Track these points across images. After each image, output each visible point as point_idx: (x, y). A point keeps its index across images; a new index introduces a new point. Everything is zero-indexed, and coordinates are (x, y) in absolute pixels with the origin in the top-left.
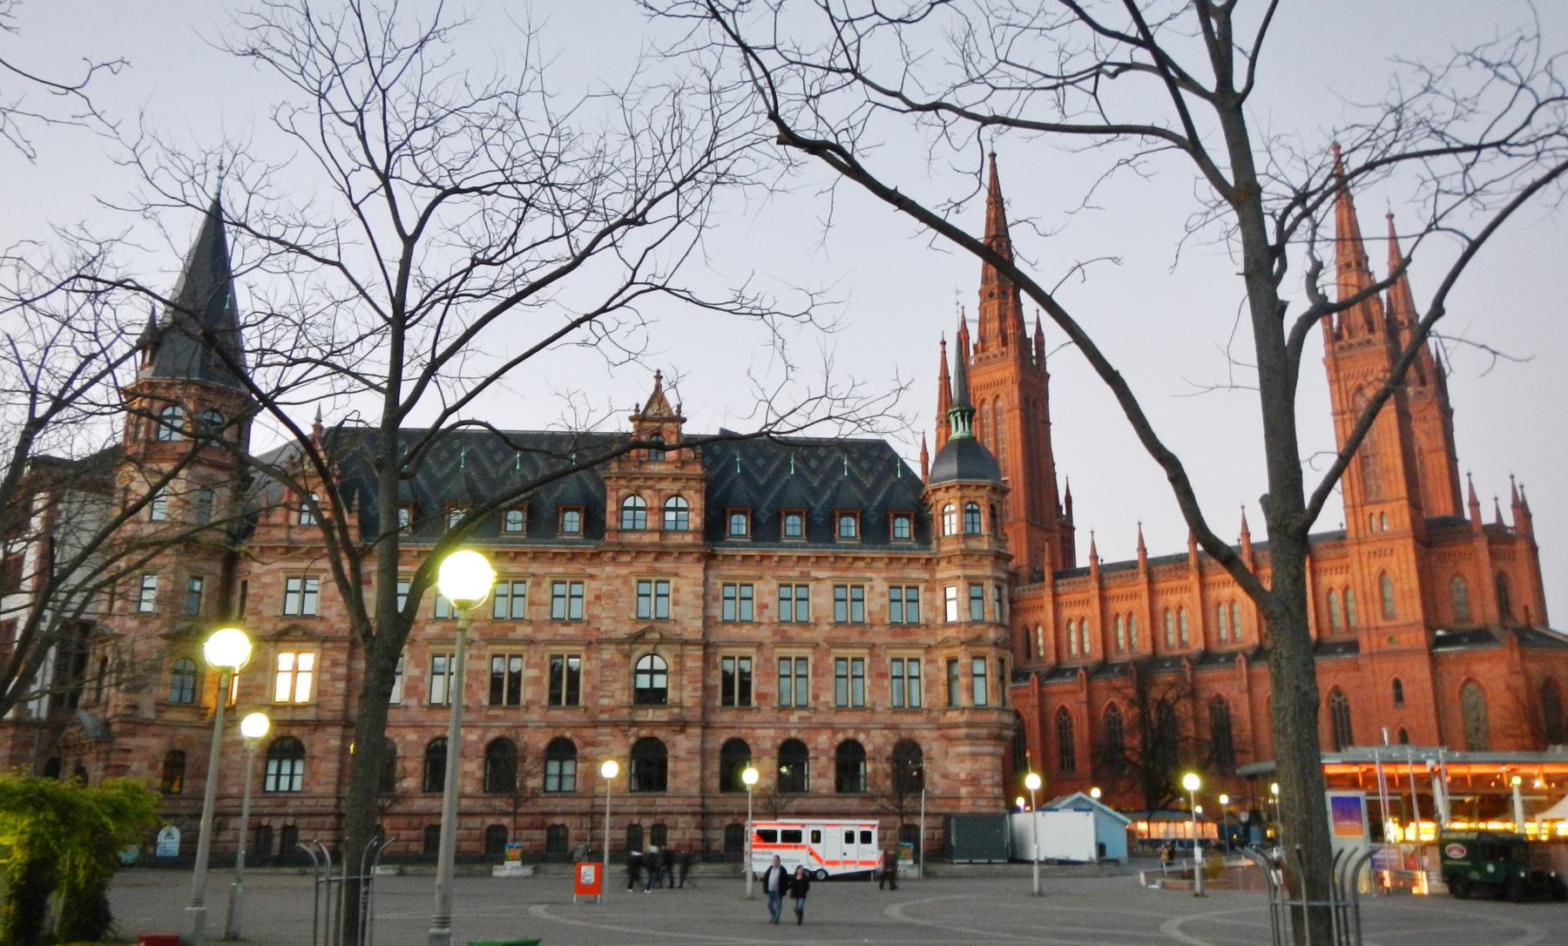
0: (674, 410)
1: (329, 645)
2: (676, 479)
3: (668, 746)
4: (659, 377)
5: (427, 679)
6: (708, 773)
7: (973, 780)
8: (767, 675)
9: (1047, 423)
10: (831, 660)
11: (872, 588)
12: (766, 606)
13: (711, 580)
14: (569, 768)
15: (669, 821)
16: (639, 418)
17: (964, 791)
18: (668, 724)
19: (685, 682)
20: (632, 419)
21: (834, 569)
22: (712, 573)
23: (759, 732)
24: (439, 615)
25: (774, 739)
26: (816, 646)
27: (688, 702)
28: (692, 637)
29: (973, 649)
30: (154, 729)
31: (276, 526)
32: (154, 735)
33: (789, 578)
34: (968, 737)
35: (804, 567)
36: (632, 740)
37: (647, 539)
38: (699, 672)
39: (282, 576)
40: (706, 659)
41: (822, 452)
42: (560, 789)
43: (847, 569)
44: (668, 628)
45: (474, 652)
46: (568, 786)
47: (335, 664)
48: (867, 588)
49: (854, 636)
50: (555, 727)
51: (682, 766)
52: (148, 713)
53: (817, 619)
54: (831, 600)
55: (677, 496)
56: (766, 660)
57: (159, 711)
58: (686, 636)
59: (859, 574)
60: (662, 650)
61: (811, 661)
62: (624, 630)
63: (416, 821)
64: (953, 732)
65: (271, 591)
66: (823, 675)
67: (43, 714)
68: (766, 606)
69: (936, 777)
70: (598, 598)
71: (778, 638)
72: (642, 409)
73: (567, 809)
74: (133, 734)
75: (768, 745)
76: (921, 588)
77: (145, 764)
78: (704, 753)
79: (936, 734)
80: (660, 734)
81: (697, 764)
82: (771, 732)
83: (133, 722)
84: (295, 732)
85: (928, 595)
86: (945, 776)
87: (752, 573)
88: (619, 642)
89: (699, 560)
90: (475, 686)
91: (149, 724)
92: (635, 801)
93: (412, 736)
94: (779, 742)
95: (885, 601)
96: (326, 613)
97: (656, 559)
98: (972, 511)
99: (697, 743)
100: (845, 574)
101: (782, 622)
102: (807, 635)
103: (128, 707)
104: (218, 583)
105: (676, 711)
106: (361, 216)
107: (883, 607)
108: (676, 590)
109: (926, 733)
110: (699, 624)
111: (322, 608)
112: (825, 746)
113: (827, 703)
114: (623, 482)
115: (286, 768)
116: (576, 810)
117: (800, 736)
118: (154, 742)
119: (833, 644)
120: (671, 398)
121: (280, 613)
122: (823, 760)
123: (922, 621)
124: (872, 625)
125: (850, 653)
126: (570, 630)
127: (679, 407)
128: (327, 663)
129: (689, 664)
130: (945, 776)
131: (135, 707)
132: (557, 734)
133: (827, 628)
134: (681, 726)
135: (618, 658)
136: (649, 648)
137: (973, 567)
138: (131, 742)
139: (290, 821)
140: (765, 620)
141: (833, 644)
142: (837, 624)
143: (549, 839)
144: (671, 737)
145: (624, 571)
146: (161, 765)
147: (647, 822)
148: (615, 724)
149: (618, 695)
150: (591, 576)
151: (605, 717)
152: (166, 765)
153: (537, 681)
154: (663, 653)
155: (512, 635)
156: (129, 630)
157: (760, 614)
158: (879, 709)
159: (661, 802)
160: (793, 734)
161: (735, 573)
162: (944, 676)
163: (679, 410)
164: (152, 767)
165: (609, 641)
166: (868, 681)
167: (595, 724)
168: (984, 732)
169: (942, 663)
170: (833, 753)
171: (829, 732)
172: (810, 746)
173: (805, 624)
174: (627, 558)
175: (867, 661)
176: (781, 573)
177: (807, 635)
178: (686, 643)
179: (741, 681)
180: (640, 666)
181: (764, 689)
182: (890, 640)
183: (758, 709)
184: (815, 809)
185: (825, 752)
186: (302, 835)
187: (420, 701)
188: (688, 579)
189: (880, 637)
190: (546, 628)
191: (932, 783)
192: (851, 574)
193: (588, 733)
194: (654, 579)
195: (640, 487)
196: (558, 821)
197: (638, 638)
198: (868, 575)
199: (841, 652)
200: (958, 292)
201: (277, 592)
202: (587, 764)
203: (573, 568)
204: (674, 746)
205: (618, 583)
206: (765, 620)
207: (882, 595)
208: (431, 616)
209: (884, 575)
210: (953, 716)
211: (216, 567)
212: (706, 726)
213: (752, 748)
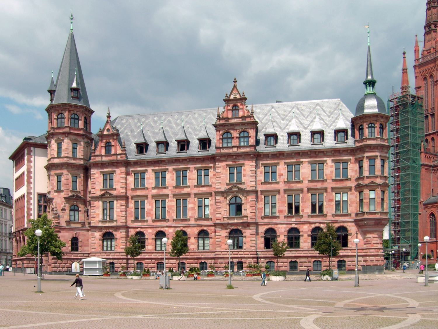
8: (282, 202)
9: (82, 74)
12: (282, 175)
24: (374, 192)
27: (250, 215)
46: (206, 248)
52: (63, 224)
54: (310, 170)
57: (67, 224)
66: (306, 202)
68: (282, 175)
72: (228, 96)
74: (60, 232)
84: (205, 228)
90: (171, 211)
91: (63, 229)
98: (74, 119)
115: (109, 243)
122: (305, 236)
128: (119, 205)
131: (59, 223)
139: (111, 261)
151: (218, 222)
153: (193, 209)
156: (55, 196)
159: (241, 254)
179: (295, 206)
181: (281, 208)
183: (279, 217)
186: (116, 265)
187: (152, 218)
200: (72, 19)
207: (332, 167)
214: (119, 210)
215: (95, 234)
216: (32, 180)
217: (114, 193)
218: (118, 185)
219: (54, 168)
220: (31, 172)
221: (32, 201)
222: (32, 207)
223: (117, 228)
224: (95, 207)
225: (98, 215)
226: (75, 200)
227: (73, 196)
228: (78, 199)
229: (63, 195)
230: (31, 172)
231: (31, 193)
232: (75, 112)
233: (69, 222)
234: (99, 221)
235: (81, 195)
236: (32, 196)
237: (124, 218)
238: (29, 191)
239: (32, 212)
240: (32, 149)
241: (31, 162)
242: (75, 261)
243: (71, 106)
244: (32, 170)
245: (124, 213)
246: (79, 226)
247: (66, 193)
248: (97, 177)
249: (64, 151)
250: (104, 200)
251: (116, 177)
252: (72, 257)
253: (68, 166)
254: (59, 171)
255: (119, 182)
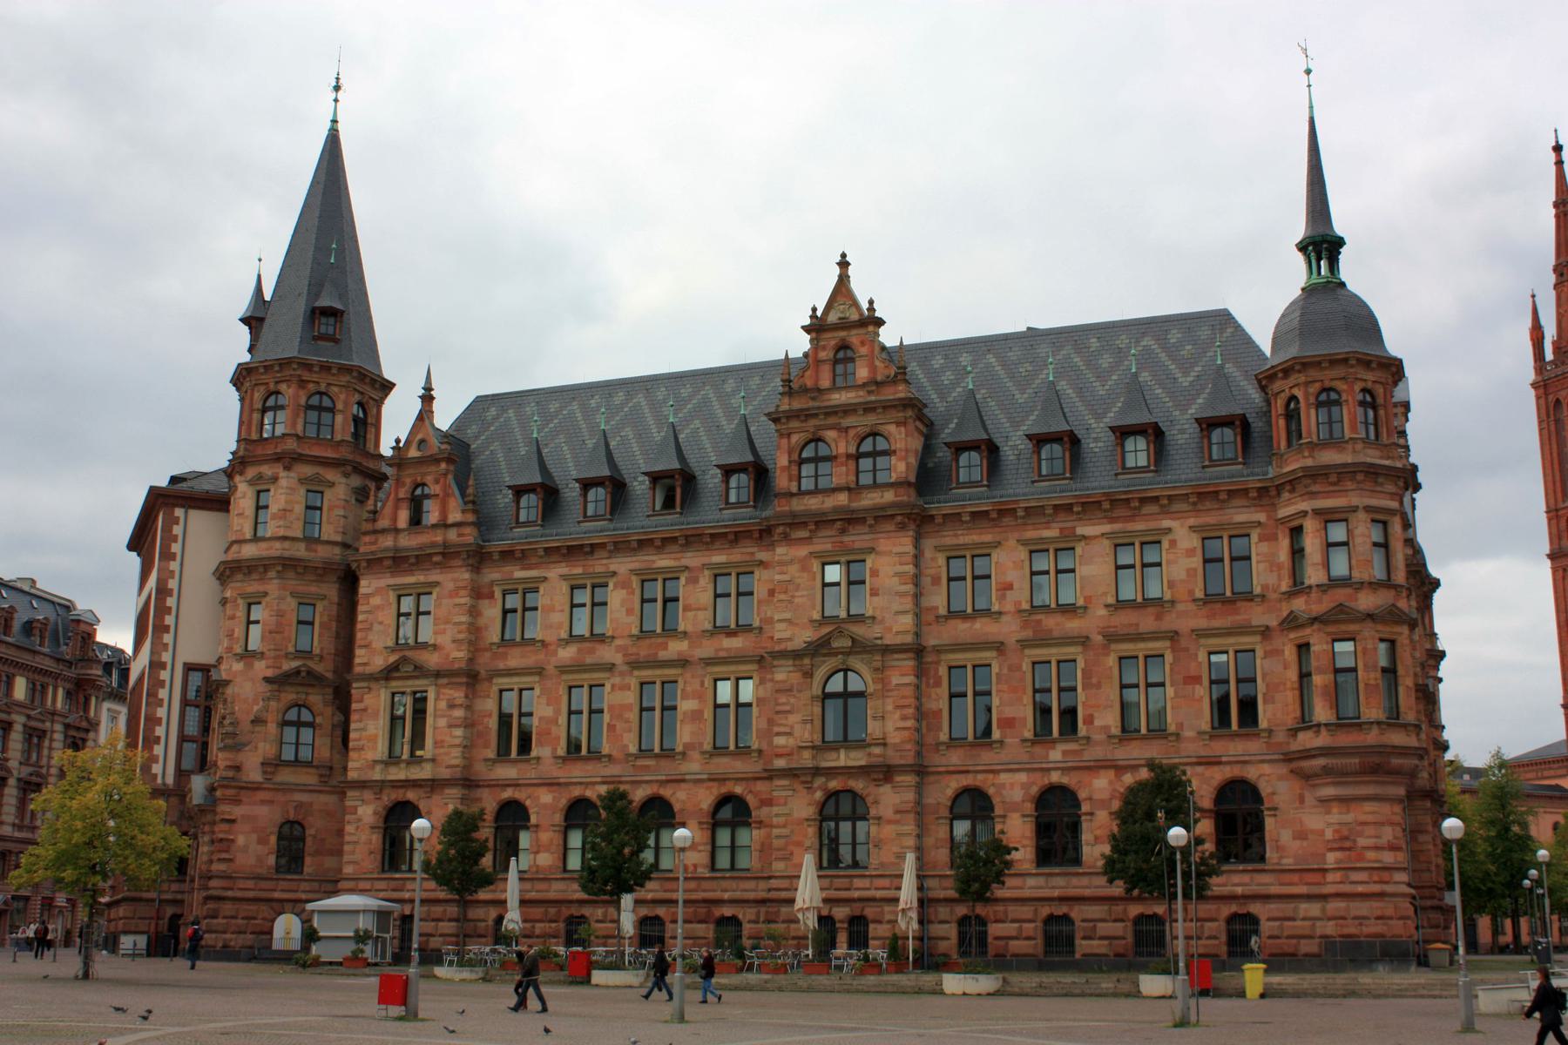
0: (865, 306)
1: (444, 681)
2: (869, 408)
3: (869, 800)
4: (844, 264)
5: (563, 720)
6: (929, 841)
7: (1344, 842)
10: (1112, 661)
11: (1173, 543)
12: (1010, 587)
13: (928, 554)
14: (744, 836)
15: (870, 912)
16: (816, 327)
17: (1331, 858)
18: (864, 771)
19: (890, 708)
20: (806, 329)
21: (1112, 520)
22: (928, 544)
23: (1003, 777)
25: (1024, 786)
26: (1084, 641)
27: (895, 738)
28: (898, 640)
29: (1331, 629)
30: (262, 795)
31: (383, 531)
32: (263, 802)
33: (1042, 540)
34: (1327, 771)
35: (1065, 522)
36: (819, 795)
37: (830, 502)
38: (909, 691)
39: (392, 597)
40: (921, 672)
41: (1123, 341)
42: (733, 868)
43: (1131, 518)
44: (859, 630)
45: (617, 680)
46: (743, 861)
47: (452, 706)
48: (1165, 544)
49: (1147, 622)
50: (722, 780)
51: (888, 831)
52: (254, 774)
53: (1088, 599)
55: (874, 434)
56: (1010, 669)
57: (265, 773)
58: (889, 640)
59: (1152, 525)
60: (854, 662)
61: (1081, 664)
62: (803, 636)
63: (552, 911)
64: (1305, 764)
65: (381, 616)
66: (1099, 685)
67: (170, 780)
68: (1010, 587)
69: (1286, 836)
70: (772, 593)
71: (1028, 633)
72: (819, 313)
73: (738, 895)
74: (237, 801)
75: (1017, 795)
76: (1254, 537)
77: (254, 837)
78: (920, 811)
79: (1282, 769)
80: (858, 785)
81: (910, 827)
82: (1022, 777)
83: (237, 787)
85: (1265, 547)
86: (1301, 835)
87: (987, 538)
88: (796, 655)
89: (902, 527)
90: (619, 726)
91: (255, 788)
92: (1041, 881)
93: (546, 797)
94: (1035, 790)
95: (1196, 562)
96: (440, 640)
97: (843, 531)
98: (320, 409)
99: (910, 796)
100: (1131, 526)
101: (1034, 608)
102: (1073, 625)
103: (229, 767)
104: (334, 610)
105: (877, 750)
106: (1311, 107)
107: (1191, 572)
108: (875, 573)
109: (1266, 768)
110: (907, 621)
111: (435, 633)
112: (1105, 796)
113: (1106, 728)
114: (795, 424)
116: (751, 895)
117: (1065, 780)
118: (263, 811)
119: (1111, 638)
120: (862, 290)
121: (391, 643)
122: (1102, 816)
123: (1257, 590)
124: (1173, 602)
125: (1141, 648)
126: (736, 643)
127: (871, 302)
128: (443, 705)
129: (896, 680)
130: (1301, 835)
131: (238, 768)
132: (724, 790)
133: (1102, 612)
134: (885, 773)
135: (796, 678)
136: (832, 663)
137: (1328, 494)
138: (237, 811)
140: (1009, 607)
141: (1111, 638)
142: (1120, 605)
143: (1138, 935)
144: (872, 789)
145: (802, 551)
146: (273, 839)
147: (841, 913)
148: (791, 773)
149: (798, 730)
150: (761, 563)
151: (780, 763)
152: (280, 838)
154: (859, 666)
155: (663, 655)
157: (1002, 598)
158: (1188, 733)
160: (1055, 777)
161: (961, 540)
162: (1293, 675)
163: (871, 309)
164: (262, 841)
165: (783, 654)
166: (1170, 691)
167: (770, 775)
168: (1355, 761)
169: (1290, 653)
170: (1029, 807)
171: (1112, 773)
172: (1082, 795)
173: (1069, 610)
174: (803, 534)
175: (1169, 658)
176: (1030, 534)
177: (1073, 625)
178: (887, 650)
180: (830, 688)
181: (1009, 712)
182: (1202, 623)
184: (1087, 892)
185: (1103, 804)
188: (890, 559)
189: (1187, 619)
190: (706, 642)
191: (1279, 848)
192: (1139, 526)
193: (761, 786)
194: (843, 559)
195: (820, 428)
196: (727, 911)
197: (819, 648)
198: (1166, 523)
199: (1127, 648)
201: (388, 616)
202: (763, 831)
203: (736, 555)
204: (876, 802)
205: (793, 570)
206: (1009, 607)
207: (1190, 552)
208: (564, 635)
209: (1192, 521)
210: (1306, 740)
211: (331, 590)
212: (921, 771)
213: (996, 801)
214: (442, 722)
215: (360, 811)
216: (169, 620)
217: (432, 660)
218: (444, 632)
219: (240, 576)
220: (169, 593)
221: (163, 694)
222: (161, 712)
223: (434, 785)
224: (365, 710)
225: (374, 739)
226: (300, 689)
227: (297, 672)
228: (312, 686)
229: (261, 668)
230: (169, 593)
231: (163, 666)
232: (323, 388)
233: (273, 765)
234: (375, 762)
235: (324, 668)
236: (165, 675)
237: (456, 752)
238: (156, 658)
239: (160, 731)
240: (179, 512)
241: (173, 557)
242: (288, 906)
243: (307, 366)
244: (173, 584)
245: (459, 732)
246: (309, 778)
247: (270, 662)
248: (378, 607)
249: (274, 517)
250: (396, 685)
251: (438, 606)
252: (277, 895)
253: (288, 565)
254: (253, 587)
255: (447, 622)
